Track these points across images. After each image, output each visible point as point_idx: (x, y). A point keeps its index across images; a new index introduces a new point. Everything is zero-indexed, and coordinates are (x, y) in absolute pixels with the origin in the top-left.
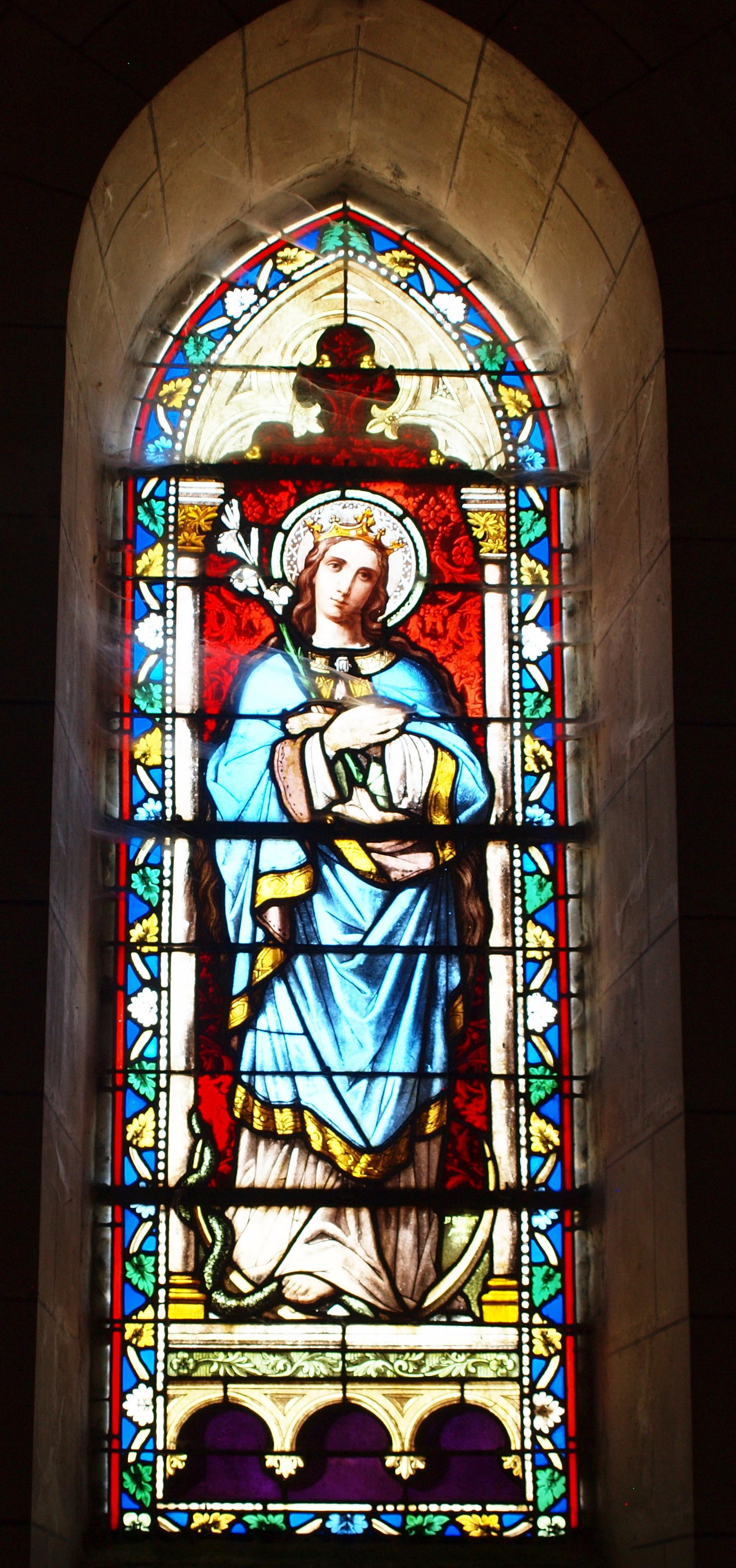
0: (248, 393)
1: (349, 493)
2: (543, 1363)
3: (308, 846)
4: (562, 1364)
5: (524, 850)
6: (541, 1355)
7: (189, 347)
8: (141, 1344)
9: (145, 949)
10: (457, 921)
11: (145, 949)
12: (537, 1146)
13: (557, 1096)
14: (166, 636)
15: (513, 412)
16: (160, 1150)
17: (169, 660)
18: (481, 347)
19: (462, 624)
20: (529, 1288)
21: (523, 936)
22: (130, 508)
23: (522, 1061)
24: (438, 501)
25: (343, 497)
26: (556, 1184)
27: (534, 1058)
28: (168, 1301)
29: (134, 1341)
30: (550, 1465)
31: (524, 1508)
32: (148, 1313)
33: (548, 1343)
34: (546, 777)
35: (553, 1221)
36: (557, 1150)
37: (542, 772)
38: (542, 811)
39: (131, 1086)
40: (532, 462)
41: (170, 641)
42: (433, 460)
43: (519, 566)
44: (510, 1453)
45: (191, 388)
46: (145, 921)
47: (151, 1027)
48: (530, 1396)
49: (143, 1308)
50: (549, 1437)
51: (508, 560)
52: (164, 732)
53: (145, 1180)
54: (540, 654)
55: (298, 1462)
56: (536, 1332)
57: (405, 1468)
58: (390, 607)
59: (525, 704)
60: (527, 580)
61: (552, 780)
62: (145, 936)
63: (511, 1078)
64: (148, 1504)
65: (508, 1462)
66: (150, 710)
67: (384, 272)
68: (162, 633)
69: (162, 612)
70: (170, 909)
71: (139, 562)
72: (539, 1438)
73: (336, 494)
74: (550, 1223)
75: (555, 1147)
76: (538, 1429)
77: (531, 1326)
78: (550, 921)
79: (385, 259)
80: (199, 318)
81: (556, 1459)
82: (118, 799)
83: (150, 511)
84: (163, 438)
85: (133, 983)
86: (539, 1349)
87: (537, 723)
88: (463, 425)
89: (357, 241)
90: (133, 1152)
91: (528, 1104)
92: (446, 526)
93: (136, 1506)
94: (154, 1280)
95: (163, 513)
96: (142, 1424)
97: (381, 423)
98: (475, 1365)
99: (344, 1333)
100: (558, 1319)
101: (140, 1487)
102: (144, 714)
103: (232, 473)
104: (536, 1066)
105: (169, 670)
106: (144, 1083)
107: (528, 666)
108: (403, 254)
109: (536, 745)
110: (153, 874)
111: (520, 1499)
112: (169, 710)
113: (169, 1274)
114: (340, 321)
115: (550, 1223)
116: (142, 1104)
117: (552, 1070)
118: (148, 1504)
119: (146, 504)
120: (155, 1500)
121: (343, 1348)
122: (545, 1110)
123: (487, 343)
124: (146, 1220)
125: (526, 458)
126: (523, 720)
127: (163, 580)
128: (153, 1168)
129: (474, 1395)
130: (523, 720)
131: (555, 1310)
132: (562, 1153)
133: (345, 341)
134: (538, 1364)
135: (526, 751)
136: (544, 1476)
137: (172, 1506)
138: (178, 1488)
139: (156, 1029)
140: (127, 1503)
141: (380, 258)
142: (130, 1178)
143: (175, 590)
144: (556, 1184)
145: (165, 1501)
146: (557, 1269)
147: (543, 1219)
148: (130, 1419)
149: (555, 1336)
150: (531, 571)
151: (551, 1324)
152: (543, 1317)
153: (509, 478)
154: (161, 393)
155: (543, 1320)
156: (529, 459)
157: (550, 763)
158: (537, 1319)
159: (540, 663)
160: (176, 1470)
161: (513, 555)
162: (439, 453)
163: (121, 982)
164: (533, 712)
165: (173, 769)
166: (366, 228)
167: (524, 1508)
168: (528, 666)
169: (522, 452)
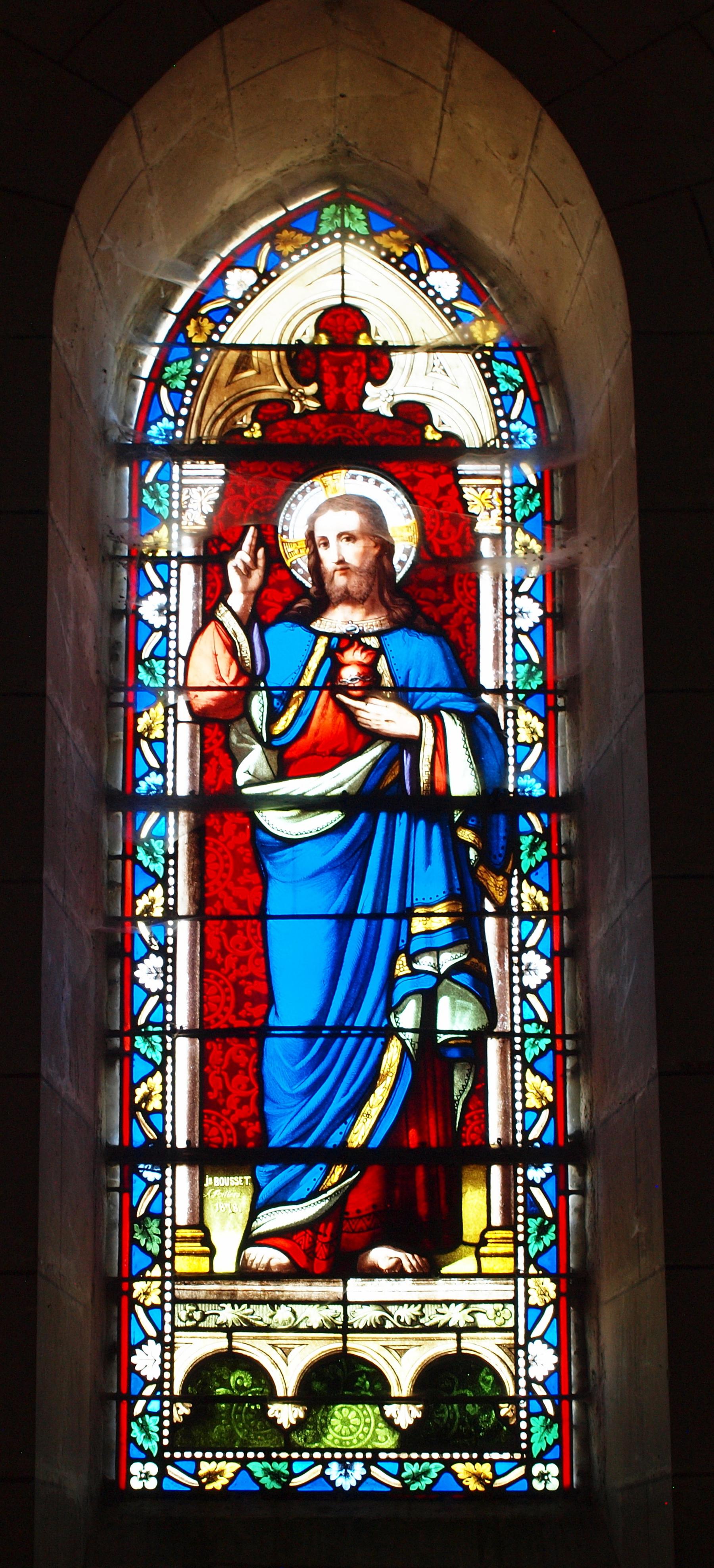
4: (556, 1315)
7: (191, 329)
10: (454, 853)
12: (524, 736)
13: (551, 1052)
15: (504, 386)
17: (172, 635)
20: (525, 1244)
21: (519, 897)
23: (517, 1020)
26: (549, 1138)
27: (529, 1014)
30: (544, 1412)
31: (517, 1456)
32: (156, 1271)
36: (550, 1106)
39: (137, 1051)
40: (525, 438)
42: (430, 435)
43: (520, 891)
45: (193, 367)
48: (519, 955)
49: (150, 1268)
50: (542, 1384)
51: (503, 535)
54: (547, 1374)
56: (531, 1282)
59: (516, 498)
60: (527, 907)
61: (545, 749)
66: (152, 685)
69: (166, 590)
70: (178, 596)
71: (140, 720)
72: (534, 1386)
77: (527, 1276)
81: (548, 1404)
82: (114, 1466)
83: (144, 1427)
84: (165, 419)
85: (139, 950)
87: (529, 694)
90: (144, 744)
91: (524, 1061)
93: (143, 1456)
96: (150, 1378)
97: (378, 400)
98: (471, 1314)
101: (155, 860)
102: (148, 689)
104: (530, 1022)
111: (516, 1449)
112: (174, 554)
113: (175, 1227)
114: (338, 301)
116: (151, 1068)
117: (546, 1026)
119: (140, 1421)
120: (162, 1448)
121: (344, 1302)
122: (538, 1066)
124: (154, 994)
125: (519, 433)
126: (516, 691)
127: (167, 560)
129: (472, 1344)
130: (516, 691)
131: (549, 1261)
132: (556, 1108)
133: (343, 320)
134: (531, 1116)
135: (517, 544)
136: (537, 1423)
138: (184, 1436)
139: (162, 993)
140: (134, 1452)
143: (178, 569)
145: (171, 1448)
147: (536, 1174)
149: (550, 1286)
151: (546, 1274)
152: (538, 1267)
156: (520, 435)
158: (532, 1270)
160: (184, 1415)
161: (509, 530)
163: (128, 950)
164: (526, 682)
167: (517, 1456)
169: (514, 427)
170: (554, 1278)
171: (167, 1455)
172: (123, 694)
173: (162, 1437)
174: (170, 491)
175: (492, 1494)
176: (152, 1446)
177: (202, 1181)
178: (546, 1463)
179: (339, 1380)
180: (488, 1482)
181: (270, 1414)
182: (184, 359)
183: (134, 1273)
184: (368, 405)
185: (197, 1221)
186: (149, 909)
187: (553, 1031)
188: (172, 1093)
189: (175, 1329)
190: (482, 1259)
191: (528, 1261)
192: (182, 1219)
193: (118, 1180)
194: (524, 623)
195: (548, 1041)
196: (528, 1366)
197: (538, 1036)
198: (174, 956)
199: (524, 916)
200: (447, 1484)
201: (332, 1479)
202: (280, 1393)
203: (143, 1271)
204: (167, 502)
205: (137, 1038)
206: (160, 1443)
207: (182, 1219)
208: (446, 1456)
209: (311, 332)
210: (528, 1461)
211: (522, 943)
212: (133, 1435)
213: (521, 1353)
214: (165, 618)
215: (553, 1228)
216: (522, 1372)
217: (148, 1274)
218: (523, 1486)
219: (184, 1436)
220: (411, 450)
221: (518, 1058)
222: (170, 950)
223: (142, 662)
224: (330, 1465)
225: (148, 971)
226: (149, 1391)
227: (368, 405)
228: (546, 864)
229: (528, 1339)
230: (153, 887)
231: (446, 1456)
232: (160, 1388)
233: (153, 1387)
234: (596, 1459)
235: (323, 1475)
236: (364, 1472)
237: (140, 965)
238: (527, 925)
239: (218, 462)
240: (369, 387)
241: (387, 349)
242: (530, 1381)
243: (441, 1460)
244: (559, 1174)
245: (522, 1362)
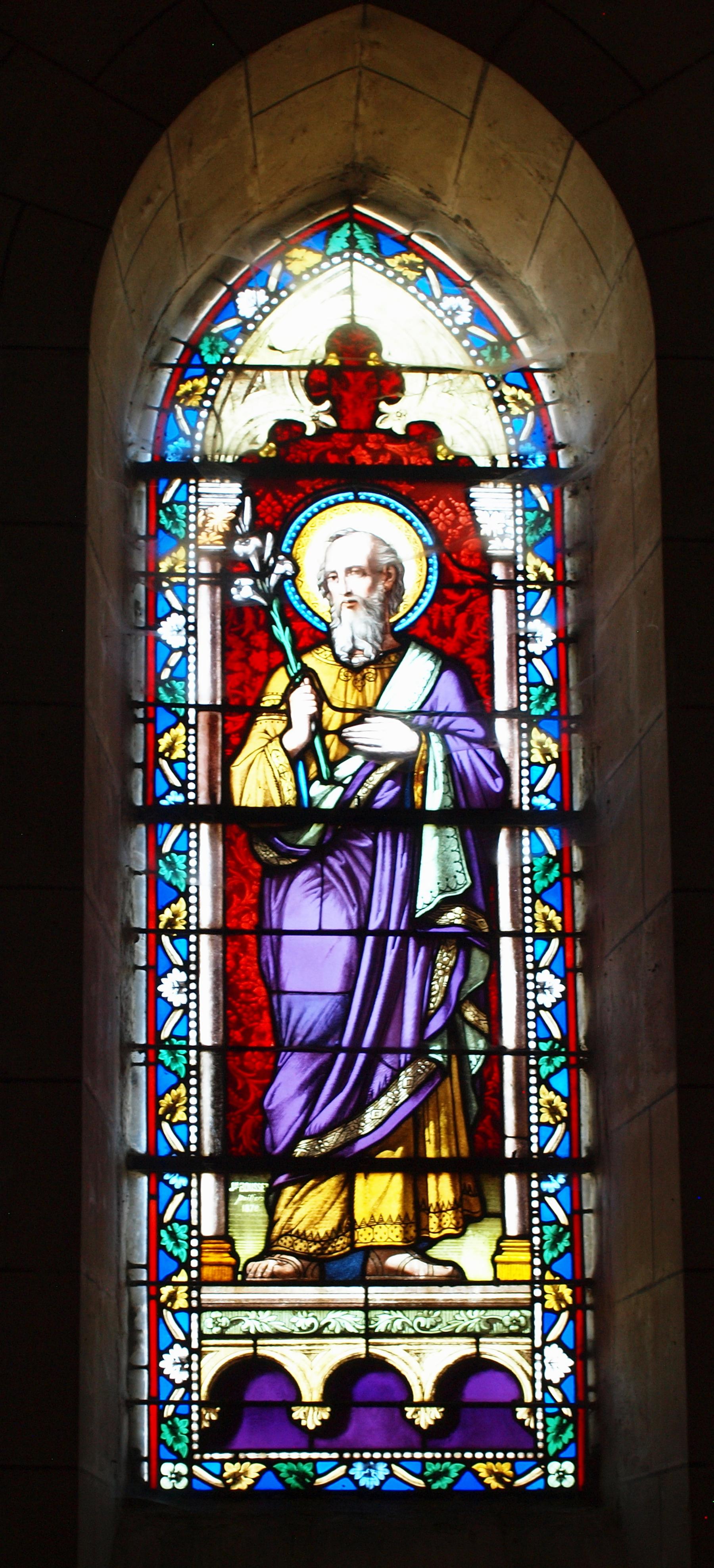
0: (262, 391)
1: (363, 495)
2: (541, 769)
3: (327, 837)
5: (525, 488)
6: (552, 1309)
8: (176, 1307)
9: (175, 580)
11: (175, 580)
14: (189, 634)
16: (190, 614)
17: (193, 1015)
18: (486, 349)
19: (470, 621)
22: (153, 513)
24: (449, 505)
25: (357, 499)
26: (563, 1152)
28: (201, 1265)
29: (167, 755)
32: (183, 1277)
33: (559, 1298)
34: (561, 1128)
35: (561, 1185)
37: (548, 764)
38: (549, 800)
39: (162, 1063)
41: (192, 640)
44: (524, 1405)
46: (172, 730)
47: (180, 649)
49: (177, 1273)
52: (188, 727)
53: (177, 1152)
55: (325, 1414)
57: (427, 1417)
58: (403, 609)
59: (545, 1238)
61: (567, 1129)
62: (173, 567)
63: (518, 935)
64: (184, 1454)
65: (522, 1413)
67: (390, 273)
68: (184, 632)
70: (196, 681)
73: (350, 495)
74: (555, 1001)
75: (557, 931)
76: (544, 1190)
78: (556, 901)
79: (393, 262)
80: (215, 316)
86: (551, 1303)
88: (471, 423)
89: (364, 242)
90: (164, 763)
92: (455, 528)
93: (174, 1457)
94: (185, 1062)
95: (184, 867)
99: (366, 1294)
100: (568, 1275)
103: (248, 470)
105: (193, 1024)
106: (175, 1060)
107: (534, 660)
108: (412, 257)
109: (538, 562)
110: (180, 860)
115: (555, 1001)
118: (184, 1454)
120: (192, 1452)
123: (492, 344)
127: (185, 934)
128: (184, 601)
137: (207, 1456)
138: (213, 1439)
141: (388, 261)
142: (163, 1151)
144: (563, 1152)
145: (201, 1451)
146: (552, 689)
148: (167, 1377)
149: (566, 1292)
150: (537, 569)
151: (563, 1281)
152: (555, 1274)
153: (516, 474)
154: (179, 393)
155: (555, 1276)
157: (565, 1114)
158: (549, 1276)
159: (545, 657)
162: (445, 447)
165: (196, 654)
166: (372, 228)
168: (534, 660)
170: (569, 1284)
171: (197, 1456)
172: (142, 710)
173: (191, 1442)
174: (187, 513)
175: (511, 1493)
176: (182, 1447)
177: (227, 1186)
178: (561, 1460)
179: (362, 1385)
180: (508, 1480)
181: (295, 1416)
182: (199, 377)
183: (162, 1277)
184: (382, 424)
185: (222, 1232)
186: (171, 922)
187: (567, 1048)
188: (197, 1120)
189: (202, 1336)
190: (498, 1266)
191: (544, 1267)
192: (209, 1228)
193: (143, 619)
194: (537, 648)
195: (563, 1059)
196: (543, 1369)
197: (552, 1053)
198: (197, 972)
199: (536, 936)
200: (468, 1483)
201: (356, 1478)
202: (306, 1398)
203: (170, 1276)
204: (184, 524)
205: (161, 1051)
206: (190, 1445)
207: (209, 1228)
208: (468, 1455)
209: (323, 351)
210: (543, 1462)
211: (536, 963)
212: (163, 1437)
213: (538, 1356)
214: (185, 996)
215: (568, 1235)
216: (538, 1376)
217: (174, 1279)
218: (540, 1485)
219: (213, 1439)
220: (426, 477)
221: (533, 1072)
222: (193, 967)
223: (163, 856)
224: (354, 1465)
225: (173, 1361)
226: (178, 1395)
227: (382, 424)
228: (558, 884)
229: (545, 1343)
230: (175, 726)
231: (468, 1455)
232: (189, 1391)
233: (182, 1390)
234: (582, 1041)
235: (347, 1475)
236: (387, 1472)
237: (165, 1356)
238: (541, 944)
239: (232, 481)
240: (383, 406)
241: (399, 369)
242: (546, 1383)
243: (462, 1460)
244: (573, 1183)
245: (538, 1366)
